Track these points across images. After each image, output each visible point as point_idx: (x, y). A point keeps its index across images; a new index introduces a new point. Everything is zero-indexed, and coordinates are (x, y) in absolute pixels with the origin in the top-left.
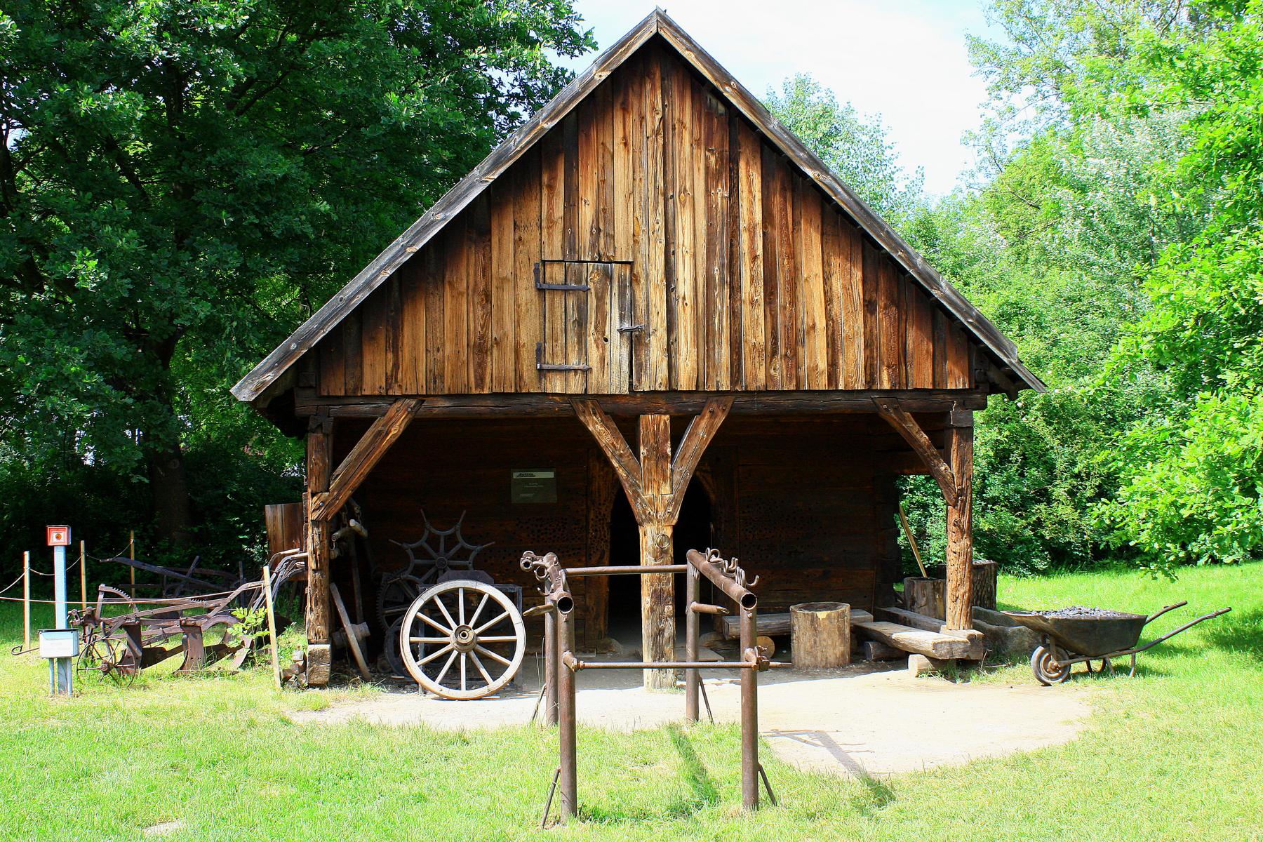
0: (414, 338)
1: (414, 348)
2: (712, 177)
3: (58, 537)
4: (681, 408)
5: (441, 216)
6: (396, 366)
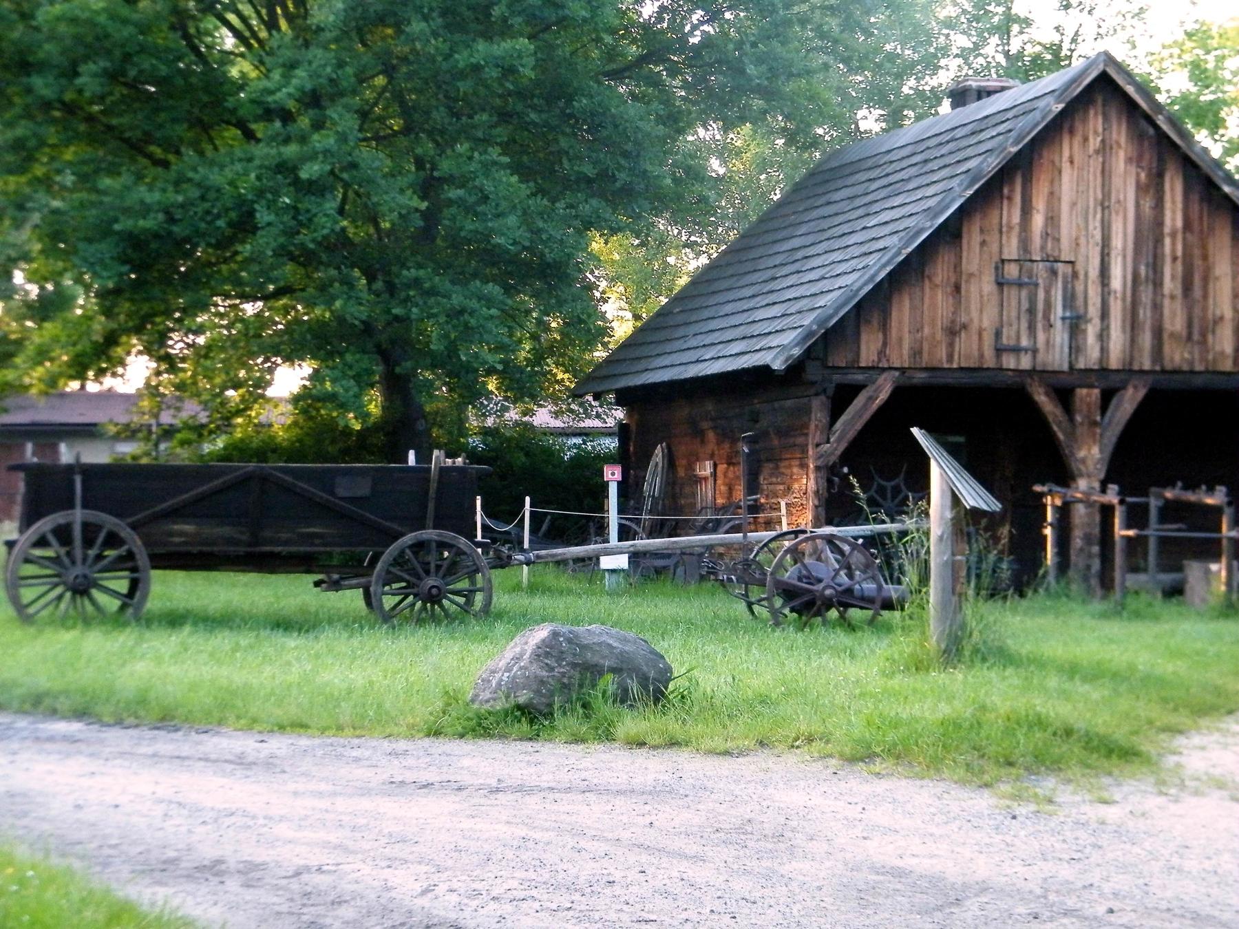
0: (900, 322)
1: (900, 330)
2: (1140, 189)
3: (613, 474)
4: (1109, 384)
5: (929, 224)
6: (885, 344)
